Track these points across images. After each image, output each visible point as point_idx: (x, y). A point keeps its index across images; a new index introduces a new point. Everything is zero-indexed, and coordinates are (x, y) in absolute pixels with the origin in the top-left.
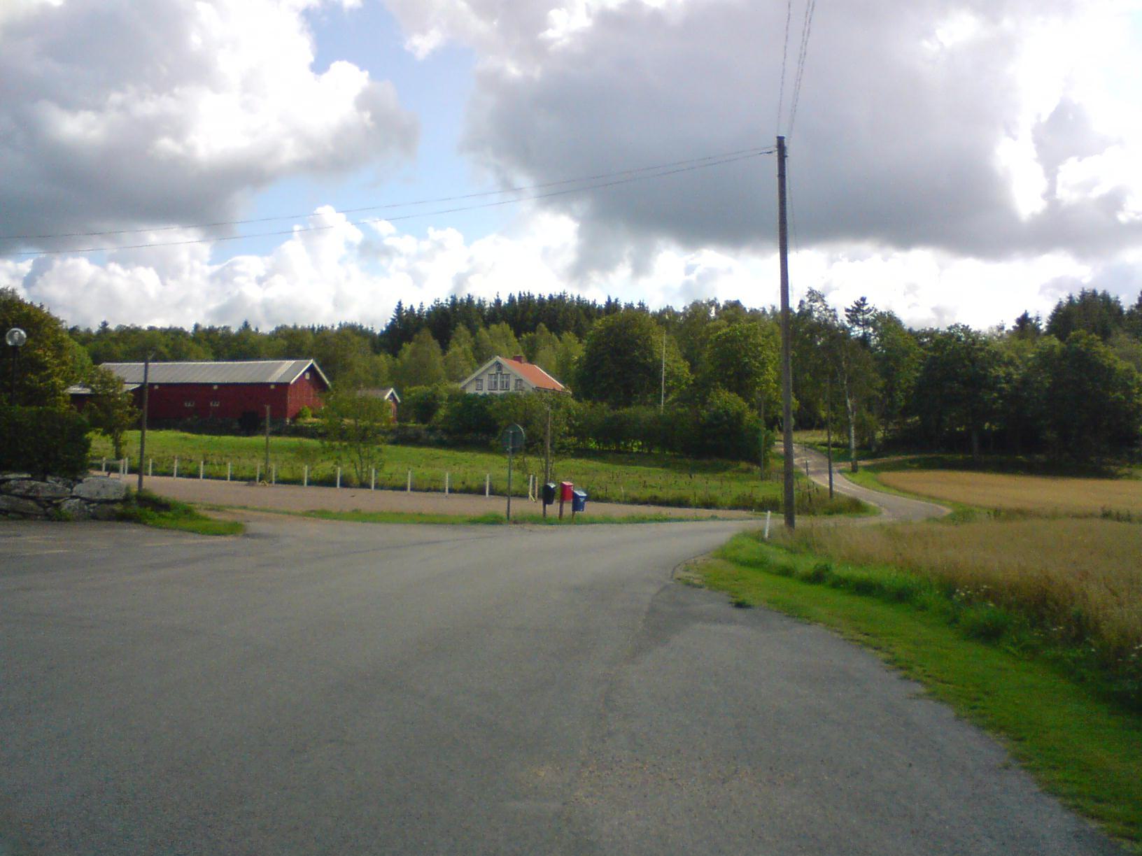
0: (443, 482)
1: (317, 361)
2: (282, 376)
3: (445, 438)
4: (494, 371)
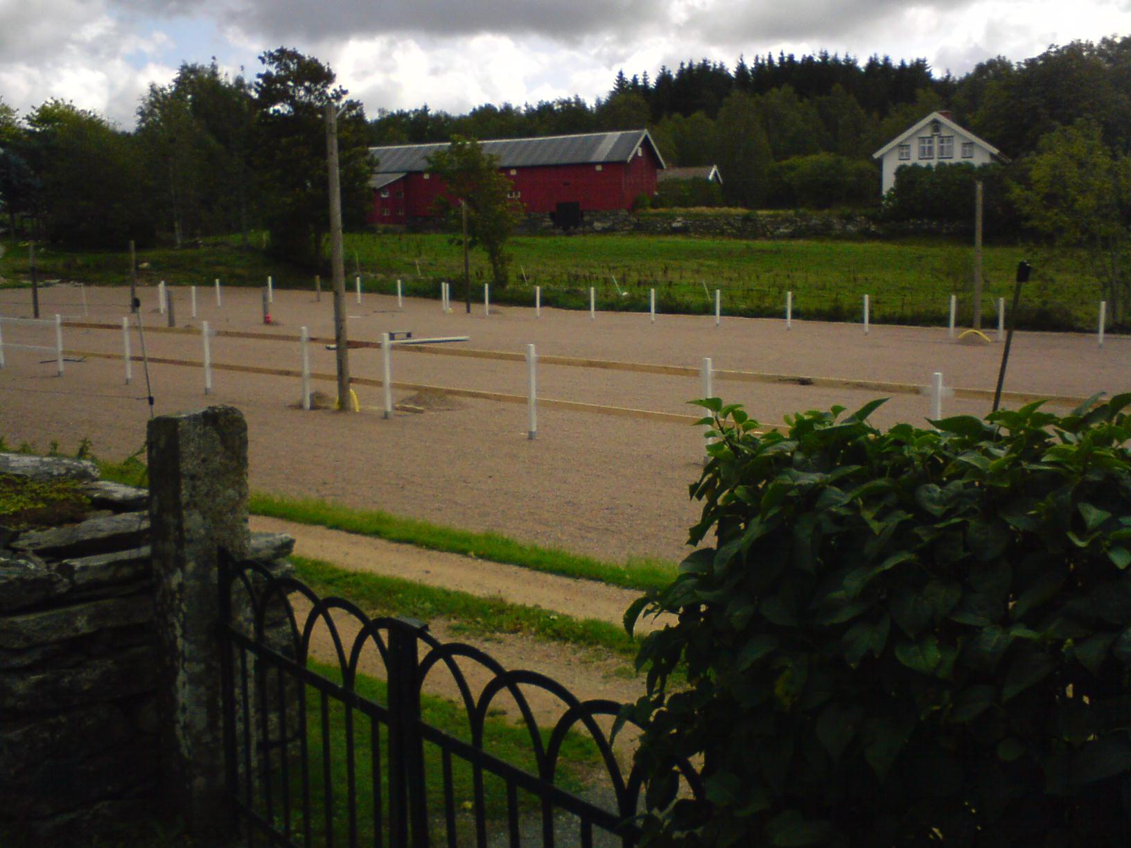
0: (222, 293)
1: (651, 133)
3: (873, 228)
4: (927, 133)
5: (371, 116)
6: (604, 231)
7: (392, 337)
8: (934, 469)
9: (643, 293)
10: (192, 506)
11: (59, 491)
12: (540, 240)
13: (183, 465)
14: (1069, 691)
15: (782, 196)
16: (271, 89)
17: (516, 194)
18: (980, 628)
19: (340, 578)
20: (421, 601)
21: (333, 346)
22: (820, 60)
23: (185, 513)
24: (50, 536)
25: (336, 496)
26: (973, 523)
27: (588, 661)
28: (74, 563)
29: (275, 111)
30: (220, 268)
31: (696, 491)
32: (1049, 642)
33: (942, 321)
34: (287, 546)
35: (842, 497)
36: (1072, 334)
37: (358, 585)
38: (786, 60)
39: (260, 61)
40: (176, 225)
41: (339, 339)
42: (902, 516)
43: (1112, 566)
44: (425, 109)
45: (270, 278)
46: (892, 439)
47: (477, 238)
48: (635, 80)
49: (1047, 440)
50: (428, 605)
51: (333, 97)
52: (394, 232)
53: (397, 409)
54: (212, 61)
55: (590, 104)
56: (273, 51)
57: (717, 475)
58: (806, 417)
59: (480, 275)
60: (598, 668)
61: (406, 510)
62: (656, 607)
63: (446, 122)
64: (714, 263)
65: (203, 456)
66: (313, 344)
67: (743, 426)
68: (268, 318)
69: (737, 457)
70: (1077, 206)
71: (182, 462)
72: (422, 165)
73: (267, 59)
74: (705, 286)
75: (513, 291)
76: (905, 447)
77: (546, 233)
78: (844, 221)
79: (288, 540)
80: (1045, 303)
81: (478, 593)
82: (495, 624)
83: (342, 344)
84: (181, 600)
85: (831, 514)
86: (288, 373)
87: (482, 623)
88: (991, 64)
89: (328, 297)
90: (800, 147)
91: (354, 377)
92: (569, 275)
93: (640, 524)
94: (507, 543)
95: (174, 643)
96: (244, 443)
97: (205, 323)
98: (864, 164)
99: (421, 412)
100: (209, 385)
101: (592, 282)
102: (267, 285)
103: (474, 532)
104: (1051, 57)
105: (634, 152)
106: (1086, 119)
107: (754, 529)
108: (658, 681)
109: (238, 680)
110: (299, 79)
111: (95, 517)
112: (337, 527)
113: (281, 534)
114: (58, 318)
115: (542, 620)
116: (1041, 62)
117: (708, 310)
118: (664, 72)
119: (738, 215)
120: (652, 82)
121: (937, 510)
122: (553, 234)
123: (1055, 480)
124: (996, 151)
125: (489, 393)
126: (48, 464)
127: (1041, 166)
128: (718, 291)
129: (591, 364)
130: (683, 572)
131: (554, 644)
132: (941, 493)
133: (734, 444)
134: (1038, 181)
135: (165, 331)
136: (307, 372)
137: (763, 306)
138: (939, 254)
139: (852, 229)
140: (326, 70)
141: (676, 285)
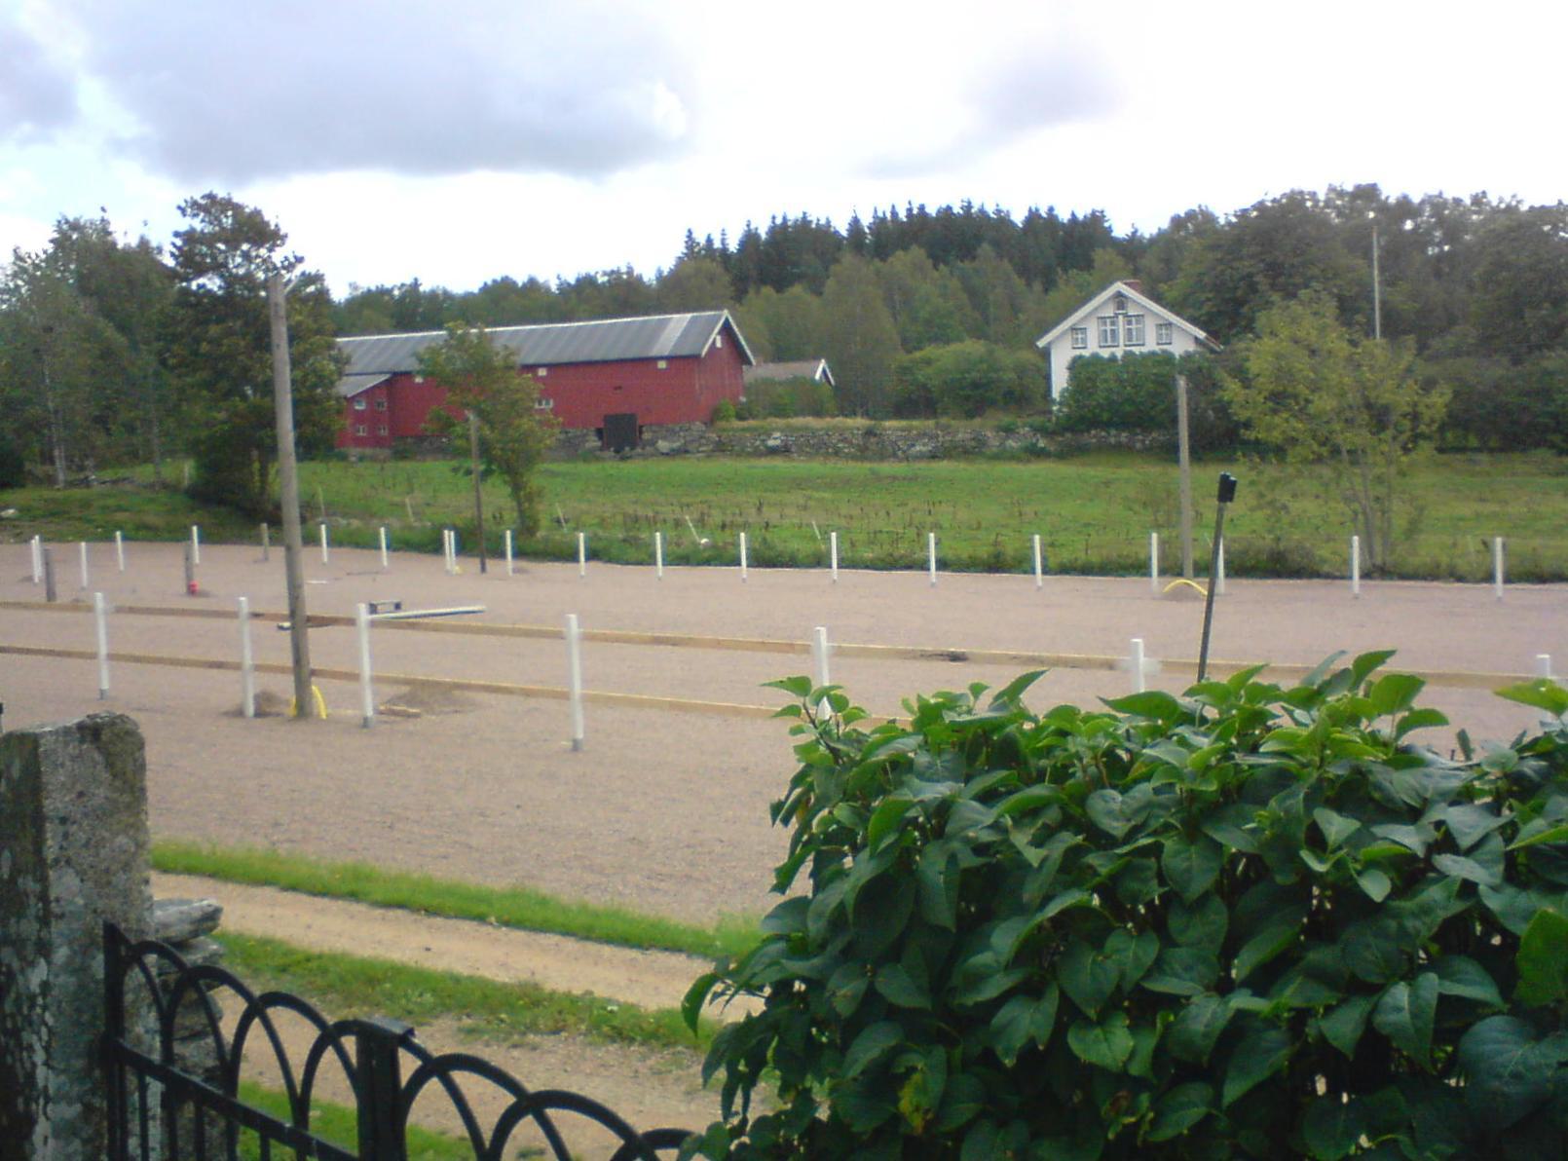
2: (675, 345)
3: (1042, 444)
4: (1109, 312)
5: (339, 294)
6: (672, 454)
7: (373, 609)
8: (1115, 770)
9: (730, 540)
10: (63, 863)
12: (582, 467)
13: (46, 802)
14: (1321, 1087)
15: (917, 403)
16: (194, 253)
17: (548, 403)
18: (1188, 998)
19: (299, 962)
20: (417, 993)
21: (287, 624)
22: (961, 212)
23: (52, 874)
25: (292, 841)
26: (1170, 844)
27: (663, 1069)
29: (200, 286)
30: (120, 516)
31: (780, 812)
32: (1286, 1015)
33: (1141, 568)
34: (211, 917)
35: (981, 814)
36: (1315, 581)
37: (324, 972)
38: (915, 211)
39: (179, 212)
40: (56, 453)
41: (293, 615)
42: (1069, 839)
43: (1366, 899)
44: (416, 284)
45: (195, 529)
46: (1053, 728)
47: (494, 467)
48: (709, 241)
49: (1270, 723)
50: (428, 997)
51: (284, 268)
52: (374, 459)
53: (382, 713)
54: (102, 214)
55: (649, 276)
56: (197, 197)
57: (810, 788)
58: (932, 701)
59: (498, 519)
60: (678, 1079)
62: (728, 988)
63: (444, 301)
64: (827, 495)
65: (79, 787)
66: (257, 622)
67: (844, 716)
68: (193, 586)
69: (837, 762)
70: (1311, 409)
71: (47, 798)
72: (409, 364)
73: (189, 210)
74: (815, 527)
75: (546, 540)
76: (1070, 738)
77: (590, 457)
78: (1003, 434)
79: (211, 909)
80: (1278, 539)
81: (503, 977)
82: (528, 1021)
83: (299, 621)
84: (45, 1008)
85: (967, 840)
86: (219, 665)
87: (508, 1021)
88: (1191, 215)
89: (278, 553)
90: (940, 335)
91: (316, 668)
92: (625, 515)
93: (735, 867)
94: (543, 902)
95: (31, 1077)
96: (141, 768)
97: (99, 595)
98: (1026, 355)
99: (416, 716)
100: (105, 686)
101: (659, 525)
102: (189, 538)
103: (497, 888)
104: (1267, 207)
105: (711, 341)
106: (1316, 291)
107: (858, 867)
108: (739, 1094)
109: (135, 1126)
110: (233, 239)
112: (293, 888)
113: (202, 900)
115: (595, 1012)
116: (1255, 214)
117: (820, 561)
118: (750, 230)
119: (858, 429)
120: (733, 246)
121: (1118, 828)
122: (598, 459)
123: (1282, 779)
124: (1202, 335)
125: (515, 685)
127: (1260, 354)
128: (834, 534)
129: (658, 641)
130: (766, 933)
131: (613, 1048)
132: (1123, 802)
133: (832, 745)
134: (1258, 375)
137: (896, 554)
138: (1132, 475)
139: (1014, 444)
140: (273, 227)
141: (775, 527)
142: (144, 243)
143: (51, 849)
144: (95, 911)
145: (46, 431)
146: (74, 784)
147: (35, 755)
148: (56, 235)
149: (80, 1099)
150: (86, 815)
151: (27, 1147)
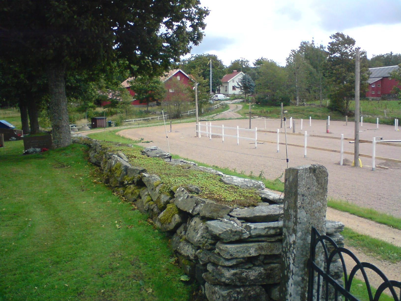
5: (370, 57)
11: (249, 193)
13: (299, 190)
16: (333, 48)
19: (356, 236)
20: (392, 253)
24: (245, 212)
28: (251, 226)
30: (311, 113)
37: (363, 240)
40: (297, 98)
41: (355, 139)
45: (329, 116)
52: (376, 100)
53: (377, 167)
61: (381, 209)
65: (308, 186)
83: (357, 141)
84: (294, 248)
86: (335, 151)
89: (353, 124)
95: (289, 266)
99: (387, 169)
110: (343, 44)
111: (262, 205)
114: (256, 129)
126: (246, 182)
135: (292, 134)
136: (342, 151)
142: (322, 47)
143: (299, 204)
144: (309, 223)
145: (295, 93)
146: (307, 185)
147: (297, 176)
148: (300, 46)
149: (301, 276)
150: (309, 194)
151: (287, 285)
